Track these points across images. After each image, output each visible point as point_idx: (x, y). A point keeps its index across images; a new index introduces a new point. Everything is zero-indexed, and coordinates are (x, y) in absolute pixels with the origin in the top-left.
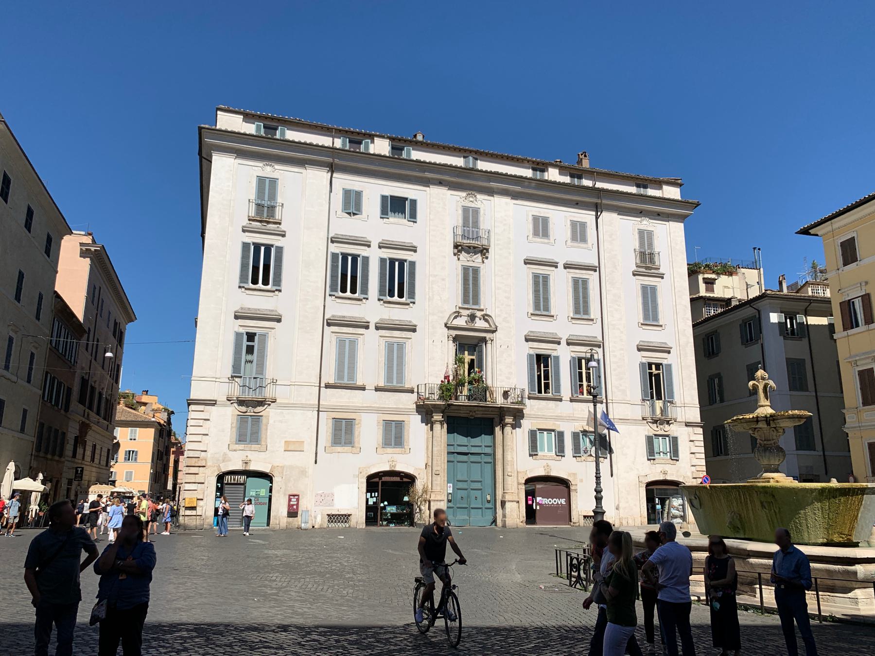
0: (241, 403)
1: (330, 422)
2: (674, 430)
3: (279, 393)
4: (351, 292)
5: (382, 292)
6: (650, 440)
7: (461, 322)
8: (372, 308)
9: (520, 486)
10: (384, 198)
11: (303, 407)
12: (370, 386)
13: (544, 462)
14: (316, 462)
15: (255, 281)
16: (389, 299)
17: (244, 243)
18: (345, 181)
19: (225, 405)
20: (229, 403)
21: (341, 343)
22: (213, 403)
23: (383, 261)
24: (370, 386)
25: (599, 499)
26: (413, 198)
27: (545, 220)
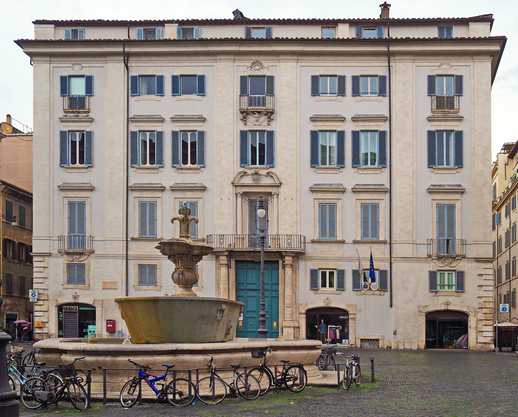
0: (68, 254)
1: (137, 267)
2: (462, 266)
3: (99, 248)
4: (192, 163)
5: (175, 160)
6: (432, 275)
7: (248, 180)
8: (168, 175)
9: (301, 316)
10: (243, 79)
11: (115, 257)
12: (349, 240)
13: (325, 296)
14: (391, 306)
15: (74, 162)
16: (183, 166)
17: (61, 132)
19: (57, 257)
20: (430, 259)
21: (143, 205)
22: (49, 255)
23: (175, 134)
24: (349, 240)
25: (289, 327)
26: (160, 74)
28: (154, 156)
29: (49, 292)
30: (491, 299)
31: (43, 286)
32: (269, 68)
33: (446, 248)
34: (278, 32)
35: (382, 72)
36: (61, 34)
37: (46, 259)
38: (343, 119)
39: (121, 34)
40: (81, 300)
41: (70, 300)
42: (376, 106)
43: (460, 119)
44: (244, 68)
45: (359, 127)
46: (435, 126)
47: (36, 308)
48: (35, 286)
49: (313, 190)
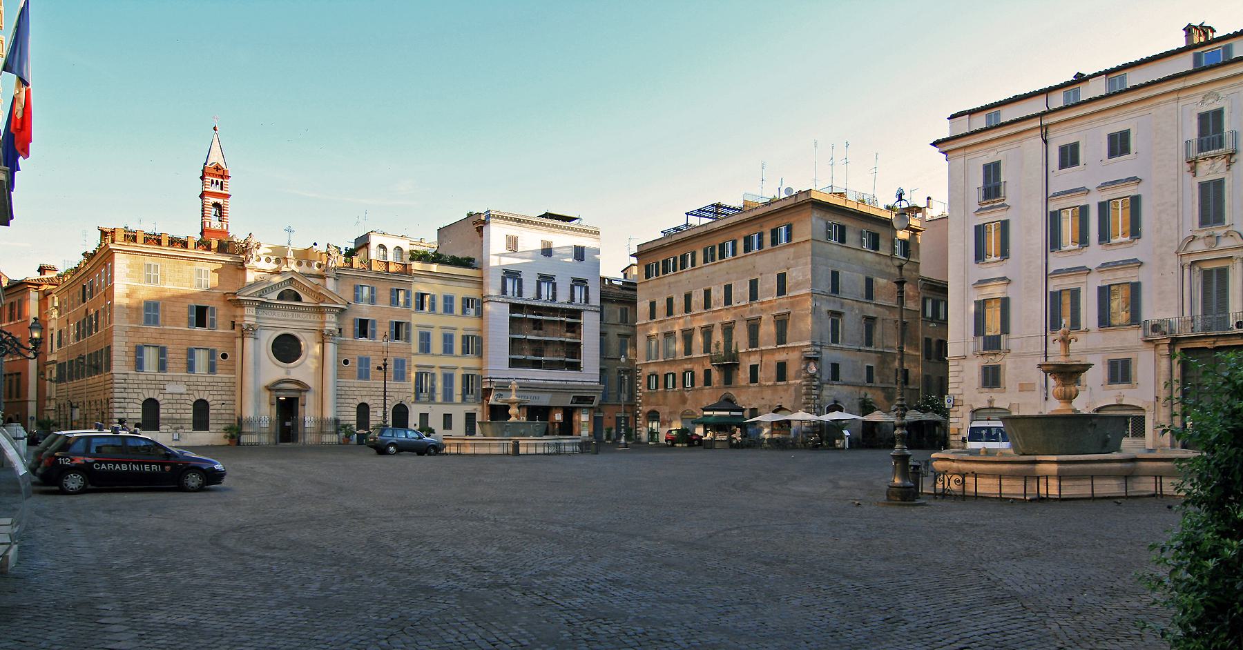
29: (964, 398)
30: (116, 405)
31: (958, 391)
36: (980, 122)
37: (962, 362)
39: (1038, 106)
45: (1105, 196)
46: (980, 221)
47: (952, 414)
48: (950, 392)
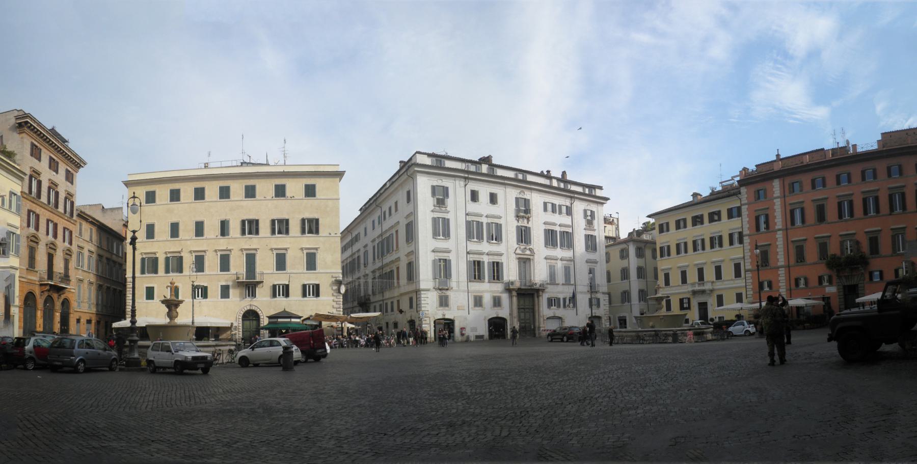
18: (472, 186)
27: (313, 186)
28: (480, 238)
32: (527, 195)
33: (592, 288)
34: (530, 178)
35: (568, 204)
38: (481, 216)
40: (447, 317)
41: (441, 317)
42: (566, 220)
43: (594, 230)
44: (436, 181)
46: (436, 215)
49: (546, 258)
